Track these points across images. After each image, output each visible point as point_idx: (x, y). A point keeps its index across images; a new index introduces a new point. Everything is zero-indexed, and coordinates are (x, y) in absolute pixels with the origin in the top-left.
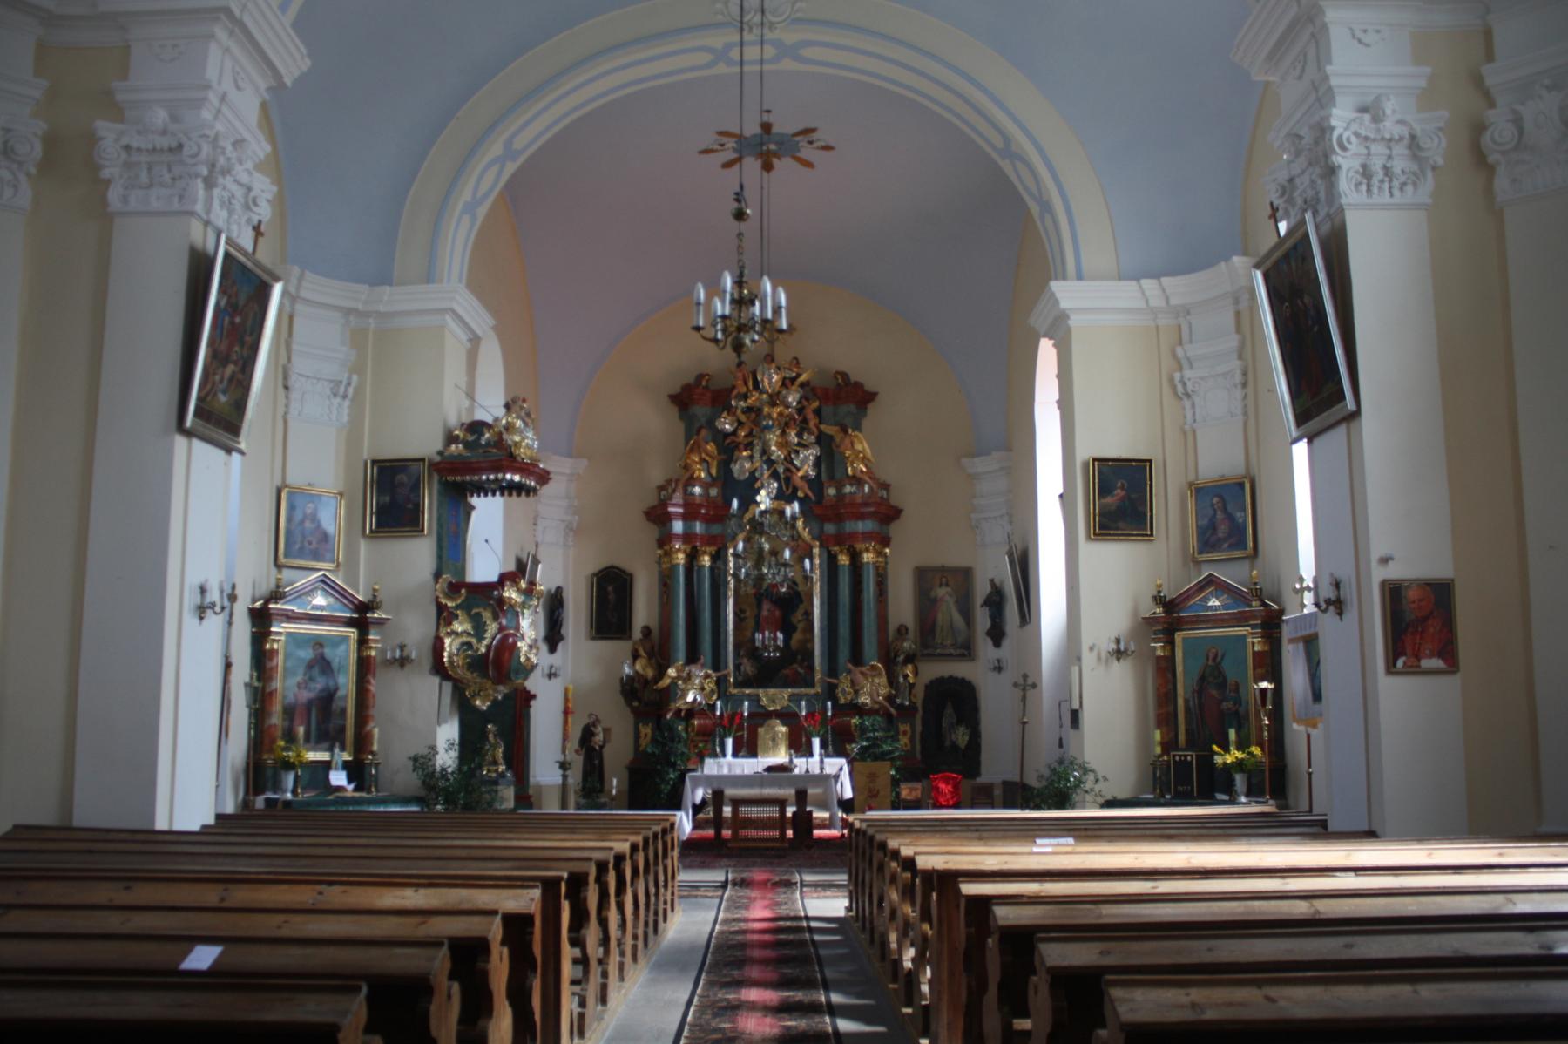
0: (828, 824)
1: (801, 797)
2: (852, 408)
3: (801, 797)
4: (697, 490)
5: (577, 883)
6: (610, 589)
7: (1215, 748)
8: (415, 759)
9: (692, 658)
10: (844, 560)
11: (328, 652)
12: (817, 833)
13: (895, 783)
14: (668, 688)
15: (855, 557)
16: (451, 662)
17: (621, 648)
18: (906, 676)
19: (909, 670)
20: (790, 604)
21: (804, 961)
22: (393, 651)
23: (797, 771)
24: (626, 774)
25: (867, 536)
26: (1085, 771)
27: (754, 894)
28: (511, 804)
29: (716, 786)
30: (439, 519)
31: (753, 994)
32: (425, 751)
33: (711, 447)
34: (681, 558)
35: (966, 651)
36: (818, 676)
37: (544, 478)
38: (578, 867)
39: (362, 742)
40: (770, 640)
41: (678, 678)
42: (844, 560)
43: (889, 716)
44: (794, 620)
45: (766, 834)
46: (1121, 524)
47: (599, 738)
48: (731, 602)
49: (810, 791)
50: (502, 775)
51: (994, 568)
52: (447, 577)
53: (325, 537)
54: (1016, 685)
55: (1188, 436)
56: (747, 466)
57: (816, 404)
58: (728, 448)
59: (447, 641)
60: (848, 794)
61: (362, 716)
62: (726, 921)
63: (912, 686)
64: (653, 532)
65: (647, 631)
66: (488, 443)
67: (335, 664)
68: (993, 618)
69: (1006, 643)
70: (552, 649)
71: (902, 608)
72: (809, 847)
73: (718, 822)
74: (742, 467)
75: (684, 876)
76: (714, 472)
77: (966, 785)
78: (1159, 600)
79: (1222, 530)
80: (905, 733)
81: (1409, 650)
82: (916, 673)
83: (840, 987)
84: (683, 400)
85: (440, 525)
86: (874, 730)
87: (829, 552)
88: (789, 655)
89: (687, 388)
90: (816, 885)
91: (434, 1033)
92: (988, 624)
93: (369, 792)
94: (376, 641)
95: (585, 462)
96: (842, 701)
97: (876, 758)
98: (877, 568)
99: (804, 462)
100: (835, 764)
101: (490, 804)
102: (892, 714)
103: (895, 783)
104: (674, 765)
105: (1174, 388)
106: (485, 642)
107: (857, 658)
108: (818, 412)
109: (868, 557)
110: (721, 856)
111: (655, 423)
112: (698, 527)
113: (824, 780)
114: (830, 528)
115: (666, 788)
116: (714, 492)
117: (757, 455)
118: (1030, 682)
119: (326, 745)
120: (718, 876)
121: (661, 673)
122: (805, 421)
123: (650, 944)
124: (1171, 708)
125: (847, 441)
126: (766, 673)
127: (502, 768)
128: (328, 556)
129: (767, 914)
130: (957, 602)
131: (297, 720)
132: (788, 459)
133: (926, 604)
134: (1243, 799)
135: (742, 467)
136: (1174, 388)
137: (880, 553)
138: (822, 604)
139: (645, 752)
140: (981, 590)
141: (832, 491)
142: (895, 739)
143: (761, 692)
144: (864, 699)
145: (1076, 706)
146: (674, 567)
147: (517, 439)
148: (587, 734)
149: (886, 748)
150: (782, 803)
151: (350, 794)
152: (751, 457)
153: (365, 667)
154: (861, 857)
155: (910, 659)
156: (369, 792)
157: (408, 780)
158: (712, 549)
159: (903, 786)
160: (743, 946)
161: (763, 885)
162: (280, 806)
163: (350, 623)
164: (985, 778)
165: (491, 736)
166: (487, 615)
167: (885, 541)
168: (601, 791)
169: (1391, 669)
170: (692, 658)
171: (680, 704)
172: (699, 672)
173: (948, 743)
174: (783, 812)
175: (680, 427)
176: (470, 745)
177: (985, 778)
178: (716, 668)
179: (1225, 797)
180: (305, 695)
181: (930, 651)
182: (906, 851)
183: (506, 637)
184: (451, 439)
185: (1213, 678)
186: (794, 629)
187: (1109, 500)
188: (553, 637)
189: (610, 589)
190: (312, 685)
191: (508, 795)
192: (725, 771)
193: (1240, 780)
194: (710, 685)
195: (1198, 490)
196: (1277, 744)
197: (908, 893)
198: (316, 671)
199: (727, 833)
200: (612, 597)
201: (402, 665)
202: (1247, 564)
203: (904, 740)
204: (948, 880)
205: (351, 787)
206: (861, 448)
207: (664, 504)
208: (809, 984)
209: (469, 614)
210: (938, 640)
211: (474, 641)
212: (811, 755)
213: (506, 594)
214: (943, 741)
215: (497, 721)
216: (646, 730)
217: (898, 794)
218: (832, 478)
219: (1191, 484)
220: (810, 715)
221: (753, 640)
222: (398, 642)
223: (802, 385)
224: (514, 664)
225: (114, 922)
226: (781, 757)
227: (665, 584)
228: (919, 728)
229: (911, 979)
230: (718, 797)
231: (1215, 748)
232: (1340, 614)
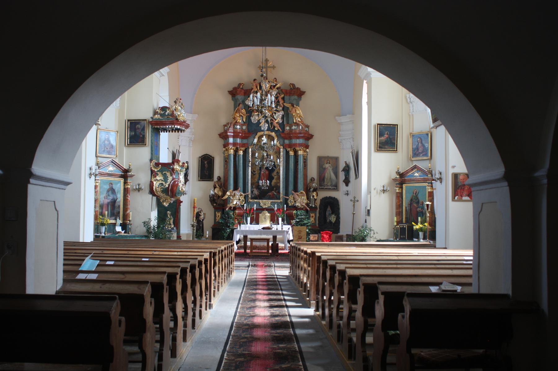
0: (284, 248)
1: (275, 238)
2: (296, 97)
3: (275, 238)
4: (238, 127)
5: (193, 267)
6: (206, 162)
7: (413, 223)
8: (144, 223)
9: (236, 188)
10: (292, 153)
11: (114, 187)
12: (280, 251)
13: (308, 234)
14: (226, 199)
15: (296, 152)
16: (156, 190)
18: (313, 196)
19: (314, 194)
21: (276, 285)
22: (136, 186)
23: (273, 229)
24: (211, 229)
25: (300, 145)
26: (371, 230)
27: (258, 269)
28: (175, 238)
29: (245, 234)
30: (151, 141)
31: (260, 291)
32: (148, 220)
33: (244, 111)
34: (232, 152)
35: (336, 187)
36: (281, 196)
37: (187, 126)
38: (192, 262)
39: (125, 217)
40: (264, 183)
41: (231, 195)
42: (292, 153)
43: (307, 211)
45: (263, 251)
46: (386, 147)
47: (202, 217)
48: (250, 168)
49: (278, 237)
50: (173, 229)
51: (346, 158)
52: (154, 161)
53: (112, 147)
54: (351, 200)
55: (411, 116)
56: (257, 118)
57: (283, 96)
59: (155, 183)
60: (291, 238)
61: (125, 209)
62: (250, 276)
63: (315, 200)
64: (221, 142)
65: (219, 178)
66: (168, 114)
67: (116, 190)
68: (346, 176)
69: (350, 185)
71: (313, 171)
72: (277, 256)
73: (245, 247)
74: (255, 119)
75: (236, 263)
76: (244, 120)
77: (334, 236)
78: (398, 173)
79: (420, 150)
80: (313, 217)
81: (459, 194)
82: (317, 195)
83: (285, 290)
84: (233, 93)
85: (152, 143)
88: (271, 188)
89: (235, 89)
90: (279, 267)
91: (145, 317)
92: (344, 178)
93: (129, 233)
94: (130, 183)
95: (197, 115)
96: (290, 205)
97: (302, 225)
99: (277, 117)
100: (287, 227)
101: (169, 238)
102: (309, 210)
103: (308, 234)
104: (229, 227)
105: (407, 100)
106: (168, 183)
107: (296, 190)
108: (283, 98)
109: (300, 153)
110: (246, 258)
111: (224, 101)
112: (238, 141)
113: (282, 232)
114: (287, 142)
115: (226, 235)
116: (244, 127)
118: (356, 199)
119: (113, 218)
120: (247, 263)
121: (224, 193)
122: (278, 102)
123: (220, 289)
124: (401, 210)
125: (294, 110)
126: (263, 194)
127: (173, 226)
128: (113, 153)
129: (263, 274)
130: (333, 169)
131: (104, 210)
132: (272, 116)
133: (321, 170)
134: (422, 240)
135: (255, 119)
136: (407, 100)
137: (305, 151)
138: (283, 169)
139: (219, 222)
140: (342, 166)
141: (288, 128)
142: (308, 219)
143: (260, 201)
144: (298, 204)
145: (369, 208)
146: (229, 155)
147: (179, 113)
148: (198, 215)
149: (305, 222)
150: (268, 240)
151: (123, 234)
152: (258, 115)
153: (126, 191)
154: (293, 256)
155: (315, 190)
156: (129, 233)
157: (142, 230)
158: (244, 149)
159: (311, 235)
160: (256, 281)
161: (262, 266)
162: (101, 237)
163: (121, 176)
164: (340, 234)
165: (169, 216)
166: (168, 174)
167: (307, 147)
168: (203, 236)
169: (453, 199)
170: (236, 188)
171: (231, 205)
172: (238, 193)
173: (328, 221)
174: (268, 244)
175: (232, 103)
176: (162, 218)
177: (340, 234)
178: (244, 192)
179: (417, 240)
180: (107, 201)
182: (305, 249)
183: (175, 182)
184: (155, 113)
185: (415, 200)
186: (273, 178)
187: (382, 138)
188: (186, 180)
189: (206, 162)
190: (109, 197)
191: (175, 235)
192: (248, 229)
193: (421, 234)
194: (242, 198)
195: (413, 136)
196: (433, 223)
197: (305, 261)
198: (110, 192)
199: (248, 251)
200: (206, 165)
201: (139, 191)
202: (428, 161)
203: (312, 219)
204: (313, 253)
205: (123, 232)
206: (299, 112)
207: (226, 132)
208: (278, 290)
209: (162, 174)
210: (326, 183)
211: (164, 183)
212: (278, 224)
213: (175, 167)
214: (326, 219)
215: (169, 211)
216: (219, 214)
217: (309, 238)
218: (288, 123)
219: (411, 134)
220: (278, 210)
221: (258, 183)
222: (137, 183)
223: (278, 88)
224: (177, 191)
225: (133, 252)
226: (267, 224)
227: (226, 161)
228: (318, 215)
229: (306, 284)
230: (245, 237)
231: (413, 223)
232: (441, 182)
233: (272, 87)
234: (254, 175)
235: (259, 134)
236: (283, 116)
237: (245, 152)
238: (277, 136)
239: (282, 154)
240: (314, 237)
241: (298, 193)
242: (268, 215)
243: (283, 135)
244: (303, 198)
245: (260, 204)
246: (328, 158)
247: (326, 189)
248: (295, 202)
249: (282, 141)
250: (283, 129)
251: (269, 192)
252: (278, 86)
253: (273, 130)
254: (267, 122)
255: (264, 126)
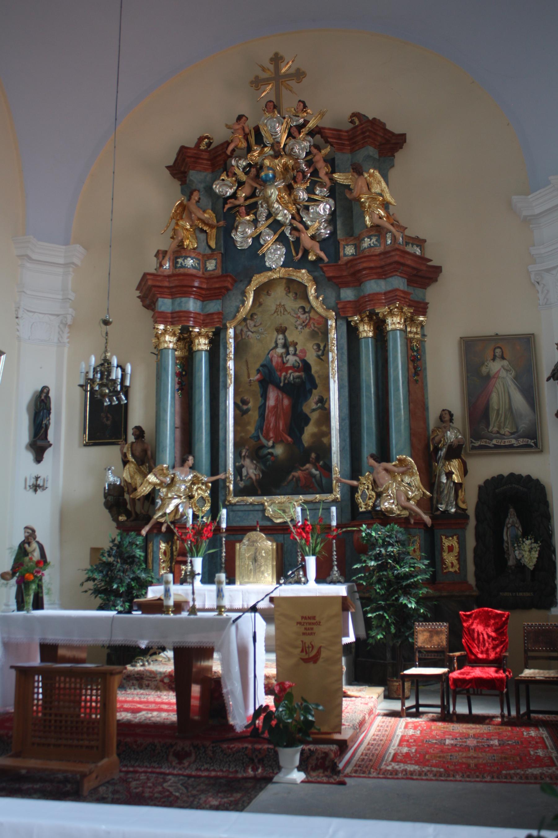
4: (190, 262)
10: (366, 331)
15: (379, 326)
17: (109, 454)
18: (449, 475)
19: (454, 466)
20: (304, 386)
25: (391, 297)
41: (161, 484)
42: (366, 331)
44: (306, 409)
58: (228, 215)
63: (458, 486)
70: (39, 459)
71: (446, 389)
76: (213, 244)
82: (465, 472)
86: (386, 545)
87: (348, 323)
98: (408, 341)
102: (433, 525)
107: (383, 454)
109: (394, 323)
111: (152, 199)
114: (348, 294)
117: (262, 219)
122: (315, 173)
126: (273, 480)
130: (516, 378)
133: (476, 382)
135: (243, 236)
155: (454, 452)
173: (511, 562)
181: (482, 443)
186: (306, 420)
223: (311, 133)
228: (471, 542)
233: (294, 130)
234: (245, 412)
235: (258, 280)
236: (333, 214)
237: (217, 342)
238: (316, 280)
239: (333, 335)
240: (434, 633)
241: (389, 466)
242: (267, 545)
243: (336, 272)
244: (407, 479)
245: (264, 510)
246: (497, 341)
247: (496, 447)
248: (379, 495)
249: (331, 294)
250: (335, 255)
251: (293, 468)
252: (311, 125)
253: (303, 262)
254: (282, 239)
255: (275, 256)
